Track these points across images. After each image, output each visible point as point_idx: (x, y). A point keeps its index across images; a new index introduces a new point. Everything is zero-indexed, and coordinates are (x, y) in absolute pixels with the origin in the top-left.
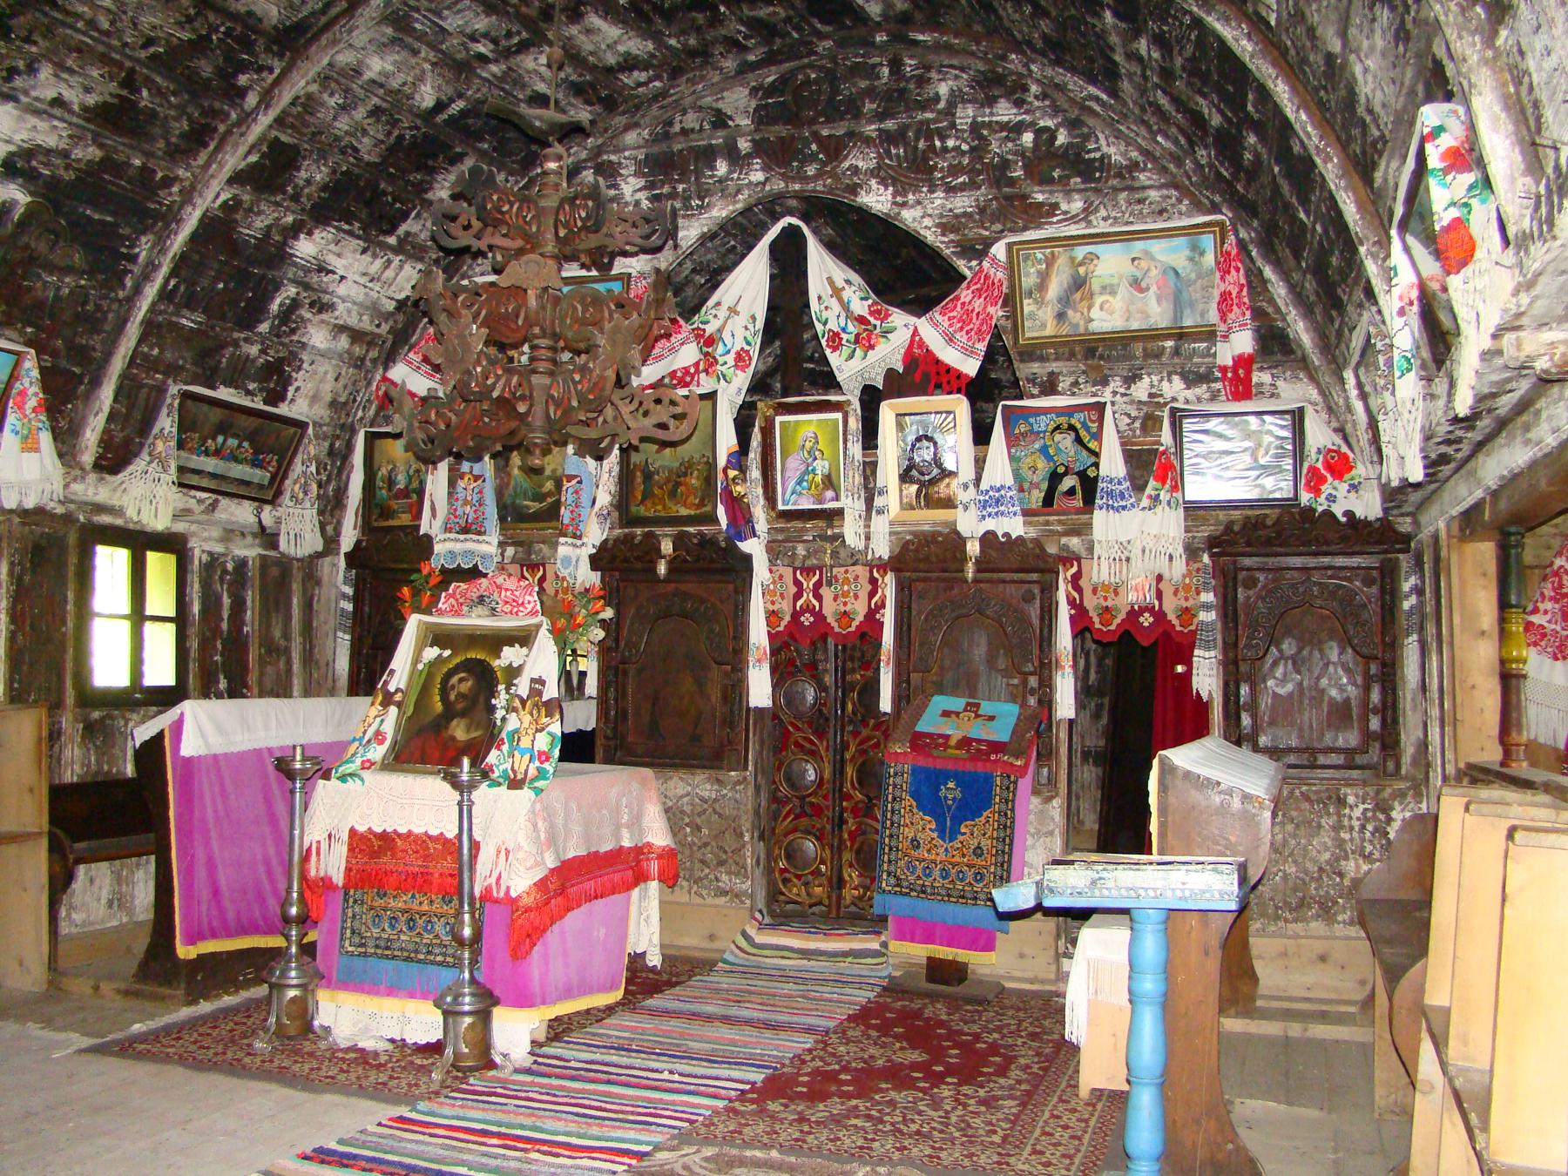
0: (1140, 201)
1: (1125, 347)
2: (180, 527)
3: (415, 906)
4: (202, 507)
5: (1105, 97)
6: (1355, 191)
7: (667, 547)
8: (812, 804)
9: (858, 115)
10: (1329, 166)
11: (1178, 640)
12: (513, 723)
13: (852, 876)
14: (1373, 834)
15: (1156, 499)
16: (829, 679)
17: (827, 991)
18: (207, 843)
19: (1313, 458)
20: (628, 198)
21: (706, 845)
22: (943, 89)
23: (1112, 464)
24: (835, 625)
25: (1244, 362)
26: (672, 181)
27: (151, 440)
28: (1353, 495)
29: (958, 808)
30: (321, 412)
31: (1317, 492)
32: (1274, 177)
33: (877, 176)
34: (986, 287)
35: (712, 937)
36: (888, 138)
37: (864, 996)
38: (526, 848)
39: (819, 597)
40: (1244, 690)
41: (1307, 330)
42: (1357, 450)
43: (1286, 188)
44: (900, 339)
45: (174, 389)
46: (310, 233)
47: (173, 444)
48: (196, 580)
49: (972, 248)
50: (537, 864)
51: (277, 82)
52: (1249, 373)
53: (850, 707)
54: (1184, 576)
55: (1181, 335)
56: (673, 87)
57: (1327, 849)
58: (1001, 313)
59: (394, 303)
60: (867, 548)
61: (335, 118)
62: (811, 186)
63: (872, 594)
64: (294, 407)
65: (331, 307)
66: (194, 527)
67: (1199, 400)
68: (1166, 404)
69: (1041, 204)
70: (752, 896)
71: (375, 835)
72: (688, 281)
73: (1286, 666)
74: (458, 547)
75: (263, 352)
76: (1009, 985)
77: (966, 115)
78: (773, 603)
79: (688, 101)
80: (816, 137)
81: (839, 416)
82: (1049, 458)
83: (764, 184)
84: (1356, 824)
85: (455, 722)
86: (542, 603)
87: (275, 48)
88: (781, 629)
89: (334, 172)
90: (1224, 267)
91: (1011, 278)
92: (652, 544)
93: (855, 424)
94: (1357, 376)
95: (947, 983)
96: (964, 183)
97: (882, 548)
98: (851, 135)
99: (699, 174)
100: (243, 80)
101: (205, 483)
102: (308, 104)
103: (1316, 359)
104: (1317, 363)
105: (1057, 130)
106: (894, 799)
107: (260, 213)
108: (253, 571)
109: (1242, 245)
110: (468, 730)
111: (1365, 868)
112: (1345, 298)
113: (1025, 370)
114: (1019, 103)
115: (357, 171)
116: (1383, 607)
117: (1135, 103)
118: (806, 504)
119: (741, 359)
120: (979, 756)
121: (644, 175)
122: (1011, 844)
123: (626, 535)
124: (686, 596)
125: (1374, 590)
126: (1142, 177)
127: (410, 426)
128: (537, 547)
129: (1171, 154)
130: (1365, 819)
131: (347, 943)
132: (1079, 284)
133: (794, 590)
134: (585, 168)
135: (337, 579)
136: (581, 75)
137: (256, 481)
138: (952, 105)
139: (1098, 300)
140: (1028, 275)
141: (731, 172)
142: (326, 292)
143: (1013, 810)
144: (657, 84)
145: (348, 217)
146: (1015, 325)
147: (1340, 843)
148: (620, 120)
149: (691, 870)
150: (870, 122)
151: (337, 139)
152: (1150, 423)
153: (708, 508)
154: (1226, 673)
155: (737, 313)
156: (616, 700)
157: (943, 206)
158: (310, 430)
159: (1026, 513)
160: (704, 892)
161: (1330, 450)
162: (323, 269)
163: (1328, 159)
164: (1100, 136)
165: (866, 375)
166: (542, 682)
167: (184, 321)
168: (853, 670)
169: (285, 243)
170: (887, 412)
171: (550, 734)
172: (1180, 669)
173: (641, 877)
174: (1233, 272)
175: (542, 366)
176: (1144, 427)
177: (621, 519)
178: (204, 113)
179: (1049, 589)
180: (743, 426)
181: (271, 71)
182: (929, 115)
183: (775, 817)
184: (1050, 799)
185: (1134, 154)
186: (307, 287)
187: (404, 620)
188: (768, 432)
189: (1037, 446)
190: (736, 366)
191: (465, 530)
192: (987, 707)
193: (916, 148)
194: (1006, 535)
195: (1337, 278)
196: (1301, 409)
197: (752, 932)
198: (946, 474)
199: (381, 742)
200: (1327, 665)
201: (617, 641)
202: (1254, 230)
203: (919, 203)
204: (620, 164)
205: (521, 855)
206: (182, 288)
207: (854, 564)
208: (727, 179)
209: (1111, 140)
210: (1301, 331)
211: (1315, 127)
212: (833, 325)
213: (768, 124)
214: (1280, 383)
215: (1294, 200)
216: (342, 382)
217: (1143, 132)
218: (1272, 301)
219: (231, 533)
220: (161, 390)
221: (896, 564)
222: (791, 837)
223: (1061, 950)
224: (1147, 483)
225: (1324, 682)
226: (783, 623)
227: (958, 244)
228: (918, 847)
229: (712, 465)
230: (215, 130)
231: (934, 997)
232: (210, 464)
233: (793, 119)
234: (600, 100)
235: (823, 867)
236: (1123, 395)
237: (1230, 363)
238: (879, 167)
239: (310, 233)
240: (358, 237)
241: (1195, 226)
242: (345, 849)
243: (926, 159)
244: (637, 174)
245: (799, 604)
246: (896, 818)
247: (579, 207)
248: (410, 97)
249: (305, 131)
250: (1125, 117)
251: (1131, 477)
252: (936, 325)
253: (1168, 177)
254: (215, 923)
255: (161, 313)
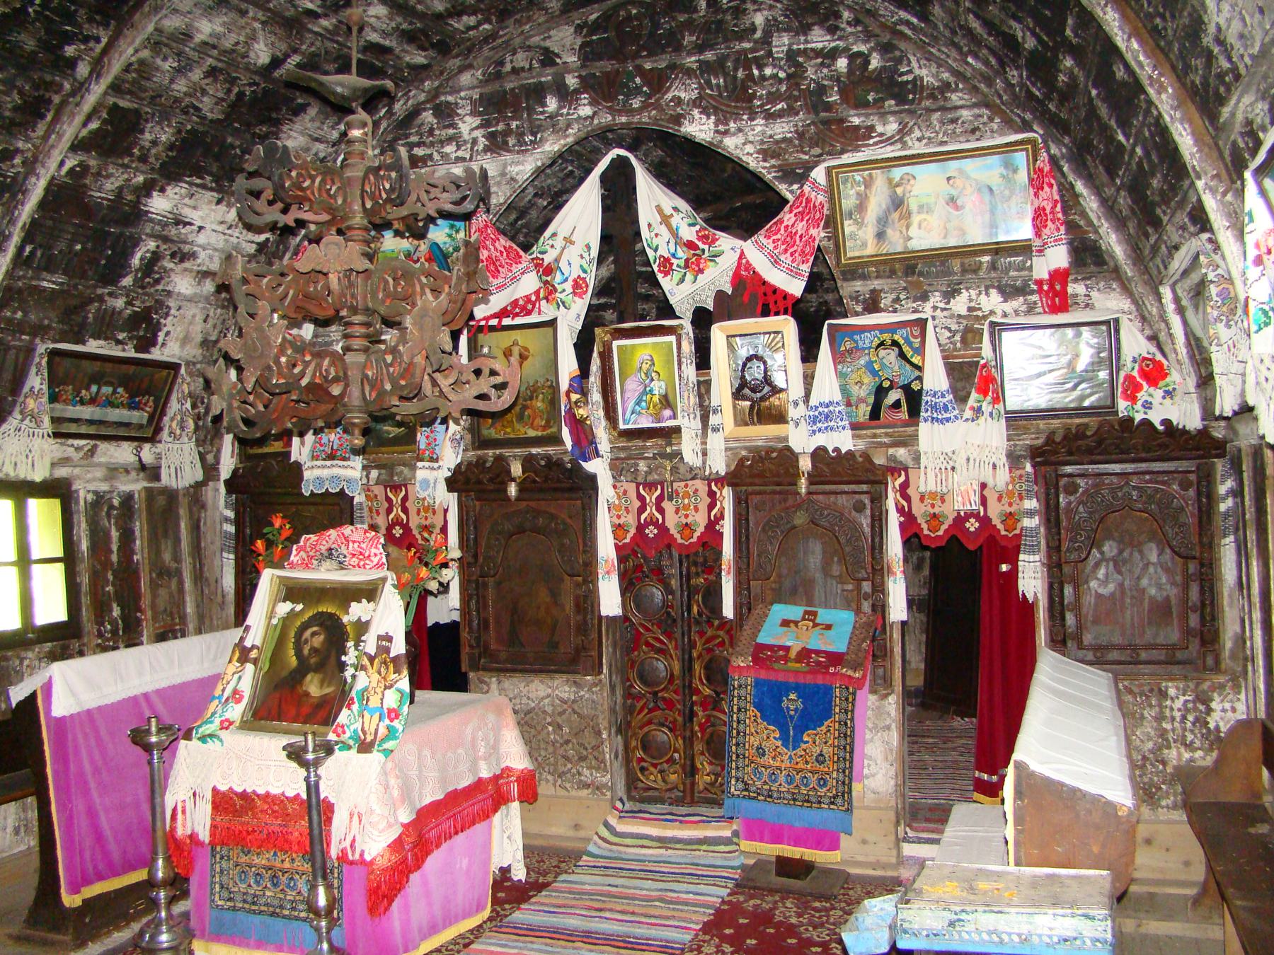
0: (954, 121)
1: (943, 264)
2: (62, 472)
3: (278, 864)
4: (81, 454)
5: (915, 21)
6: (1191, 123)
7: (516, 469)
8: (664, 699)
9: (678, 48)
10: (1164, 96)
11: (1003, 543)
12: (362, 681)
13: (704, 764)
14: (1194, 724)
15: (978, 411)
16: (674, 583)
17: (682, 889)
18: (86, 792)
19: (1129, 367)
20: (466, 137)
21: (567, 742)
22: (759, 19)
23: (935, 379)
24: (677, 536)
25: (1059, 276)
26: (505, 118)
27: (21, 399)
28: (1168, 401)
29: (801, 717)
30: (193, 352)
31: (1134, 399)
32: (1091, 99)
33: (700, 106)
34: (807, 210)
35: (577, 827)
36: (706, 68)
37: (717, 894)
38: (378, 811)
39: (661, 511)
40: (1068, 590)
41: (1119, 242)
42: (1172, 356)
43: (1103, 111)
44: (728, 262)
45: (42, 347)
46: (162, 190)
47: (45, 399)
48: (83, 519)
49: (793, 171)
50: (390, 826)
51: (105, 52)
52: (1065, 285)
53: (695, 609)
54: (1007, 484)
55: (998, 250)
56: (502, 29)
57: (1150, 739)
58: (823, 234)
59: (254, 246)
60: (704, 463)
61: (172, 81)
62: (637, 118)
63: (711, 507)
64: (166, 351)
65: (193, 255)
66: (77, 471)
67: (1017, 313)
68: (985, 317)
69: (857, 128)
70: (612, 789)
71: (236, 794)
72: (531, 204)
73: (1107, 568)
74: (325, 473)
75: (129, 303)
76: (853, 871)
77: (781, 43)
78: (619, 517)
79: (517, 41)
80: (640, 71)
81: (672, 338)
82: (874, 373)
83: (592, 118)
84: (1177, 715)
85: (309, 677)
86: (388, 556)
87: (98, 18)
88: (627, 541)
89: (179, 132)
90: (1037, 183)
91: (831, 200)
92: (501, 466)
93: (688, 347)
94: (1174, 291)
95: (796, 877)
96: (782, 110)
97: (719, 464)
98: (673, 67)
99: (530, 111)
100: (70, 51)
101: (84, 429)
102: (143, 69)
103: (1129, 271)
104: (1130, 274)
105: (870, 55)
106: (739, 710)
107: (108, 177)
108: (139, 504)
109: (1053, 160)
110: (321, 687)
111: (1187, 755)
112: (1165, 219)
113: (848, 289)
114: (832, 30)
115: (201, 129)
116: (1200, 510)
117: (946, 26)
118: (646, 423)
119: (578, 286)
120: (821, 668)
121: (480, 114)
122: (852, 752)
123: (479, 458)
124: (538, 513)
125: (1191, 492)
126: (954, 97)
127: (230, 406)
128: (399, 469)
129: (981, 74)
130: (1185, 710)
131: (217, 898)
132: (897, 203)
133: (638, 504)
134: (425, 110)
135: (220, 503)
136: (411, 23)
137: (134, 421)
138: (768, 34)
139: (916, 219)
140: (847, 197)
141: (561, 108)
142: (185, 242)
143: (852, 720)
144: (487, 26)
145: (198, 172)
146: (837, 246)
147: (1163, 733)
148: (454, 63)
149: (556, 764)
150: (690, 54)
151: (177, 100)
152: (970, 336)
153: (554, 430)
154: (1050, 575)
155: (572, 243)
156: (478, 611)
157: (763, 133)
158: (183, 371)
159: (855, 427)
160: (568, 785)
161: (1144, 359)
162: (179, 222)
163: (1161, 89)
164: (912, 58)
165: (697, 298)
166: (389, 639)
167: (45, 284)
168: (697, 574)
169: (139, 202)
170: (718, 334)
171: (398, 690)
172: (1004, 567)
173: (500, 799)
174: (1046, 188)
175: (357, 343)
176: (963, 340)
177: (473, 443)
178: (36, 87)
179: (878, 500)
180: (583, 346)
181: (98, 40)
182: (747, 45)
183: (629, 710)
184: (886, 696)
185: (946, 76)
186: (166, 239)
187: (258, 573)
188: (606, 356)
189: (862, 362)
190: (574, 293)
191: (331, 457)
192: (824, 615)
193: (735, 77)
194: (837, 450)
195: (1157, 199)
196: (1117, 321)
197: (613, 821)
198: (776, 390)
199: (238, 701)
200: (1148, 564)
201: (476, 556)
202: (1065, 145)
203: (740, 130)
204: (456, 104)
205: (375, 818)
206: (39, 254)
207: (693, 479)
208: (557, 115)
209: (922, 62)
210: (1113, 243)
211: (1148, 57)
212: (663, 252)
213: (593, 60)
214: (1094, 294)
215: (1113, 123)
216: (211, 322)
217: (954, 53)
218: (1083, 214)
219: (114, 471)
220: (30, 350)
221: (733, 478)
222: (646, 729)
223: (901, 835)
224: (969, 395)
225: (1144, 582)
226: (630, 535)
227: (779, 168)
228: (764, 755)
229: (555, 388)
230: (50, 101)
231: (786, 893)
232: (87, 412)
233: (619, 55)
234: (433, 46)
235: (676, 755)
236: (943, 310)
237: (1046, 276)
238: (701, 98)
239: (162, 190)
240: (212, 189)
241: (1007, 145)
242: (209, 807)
243: (745, 88)
244: (474, 113)
245: (643, 517)
246: (741, 727)
247: (383, 178)
248: (245, 56)
249: (143, 95)
250: (936, 39)
251: (954, 389)
252: (761, 247)
253: (980, 97)
254: (101, 866)
255: (19, 278)
